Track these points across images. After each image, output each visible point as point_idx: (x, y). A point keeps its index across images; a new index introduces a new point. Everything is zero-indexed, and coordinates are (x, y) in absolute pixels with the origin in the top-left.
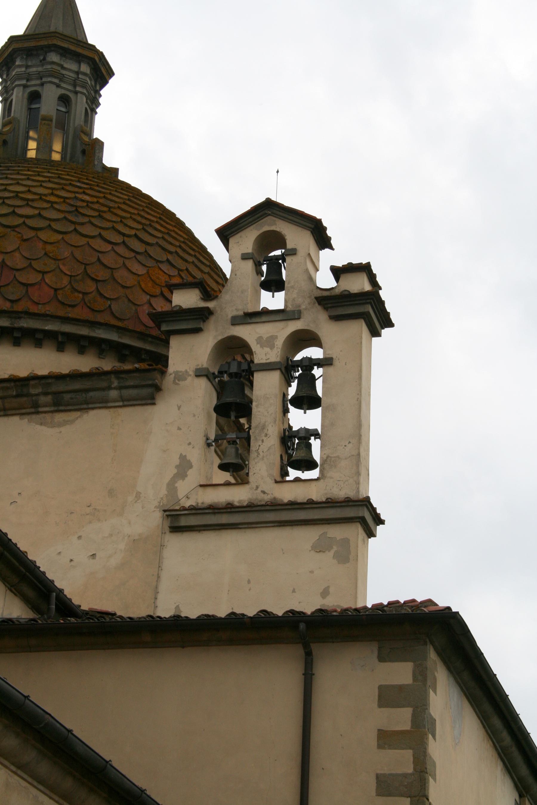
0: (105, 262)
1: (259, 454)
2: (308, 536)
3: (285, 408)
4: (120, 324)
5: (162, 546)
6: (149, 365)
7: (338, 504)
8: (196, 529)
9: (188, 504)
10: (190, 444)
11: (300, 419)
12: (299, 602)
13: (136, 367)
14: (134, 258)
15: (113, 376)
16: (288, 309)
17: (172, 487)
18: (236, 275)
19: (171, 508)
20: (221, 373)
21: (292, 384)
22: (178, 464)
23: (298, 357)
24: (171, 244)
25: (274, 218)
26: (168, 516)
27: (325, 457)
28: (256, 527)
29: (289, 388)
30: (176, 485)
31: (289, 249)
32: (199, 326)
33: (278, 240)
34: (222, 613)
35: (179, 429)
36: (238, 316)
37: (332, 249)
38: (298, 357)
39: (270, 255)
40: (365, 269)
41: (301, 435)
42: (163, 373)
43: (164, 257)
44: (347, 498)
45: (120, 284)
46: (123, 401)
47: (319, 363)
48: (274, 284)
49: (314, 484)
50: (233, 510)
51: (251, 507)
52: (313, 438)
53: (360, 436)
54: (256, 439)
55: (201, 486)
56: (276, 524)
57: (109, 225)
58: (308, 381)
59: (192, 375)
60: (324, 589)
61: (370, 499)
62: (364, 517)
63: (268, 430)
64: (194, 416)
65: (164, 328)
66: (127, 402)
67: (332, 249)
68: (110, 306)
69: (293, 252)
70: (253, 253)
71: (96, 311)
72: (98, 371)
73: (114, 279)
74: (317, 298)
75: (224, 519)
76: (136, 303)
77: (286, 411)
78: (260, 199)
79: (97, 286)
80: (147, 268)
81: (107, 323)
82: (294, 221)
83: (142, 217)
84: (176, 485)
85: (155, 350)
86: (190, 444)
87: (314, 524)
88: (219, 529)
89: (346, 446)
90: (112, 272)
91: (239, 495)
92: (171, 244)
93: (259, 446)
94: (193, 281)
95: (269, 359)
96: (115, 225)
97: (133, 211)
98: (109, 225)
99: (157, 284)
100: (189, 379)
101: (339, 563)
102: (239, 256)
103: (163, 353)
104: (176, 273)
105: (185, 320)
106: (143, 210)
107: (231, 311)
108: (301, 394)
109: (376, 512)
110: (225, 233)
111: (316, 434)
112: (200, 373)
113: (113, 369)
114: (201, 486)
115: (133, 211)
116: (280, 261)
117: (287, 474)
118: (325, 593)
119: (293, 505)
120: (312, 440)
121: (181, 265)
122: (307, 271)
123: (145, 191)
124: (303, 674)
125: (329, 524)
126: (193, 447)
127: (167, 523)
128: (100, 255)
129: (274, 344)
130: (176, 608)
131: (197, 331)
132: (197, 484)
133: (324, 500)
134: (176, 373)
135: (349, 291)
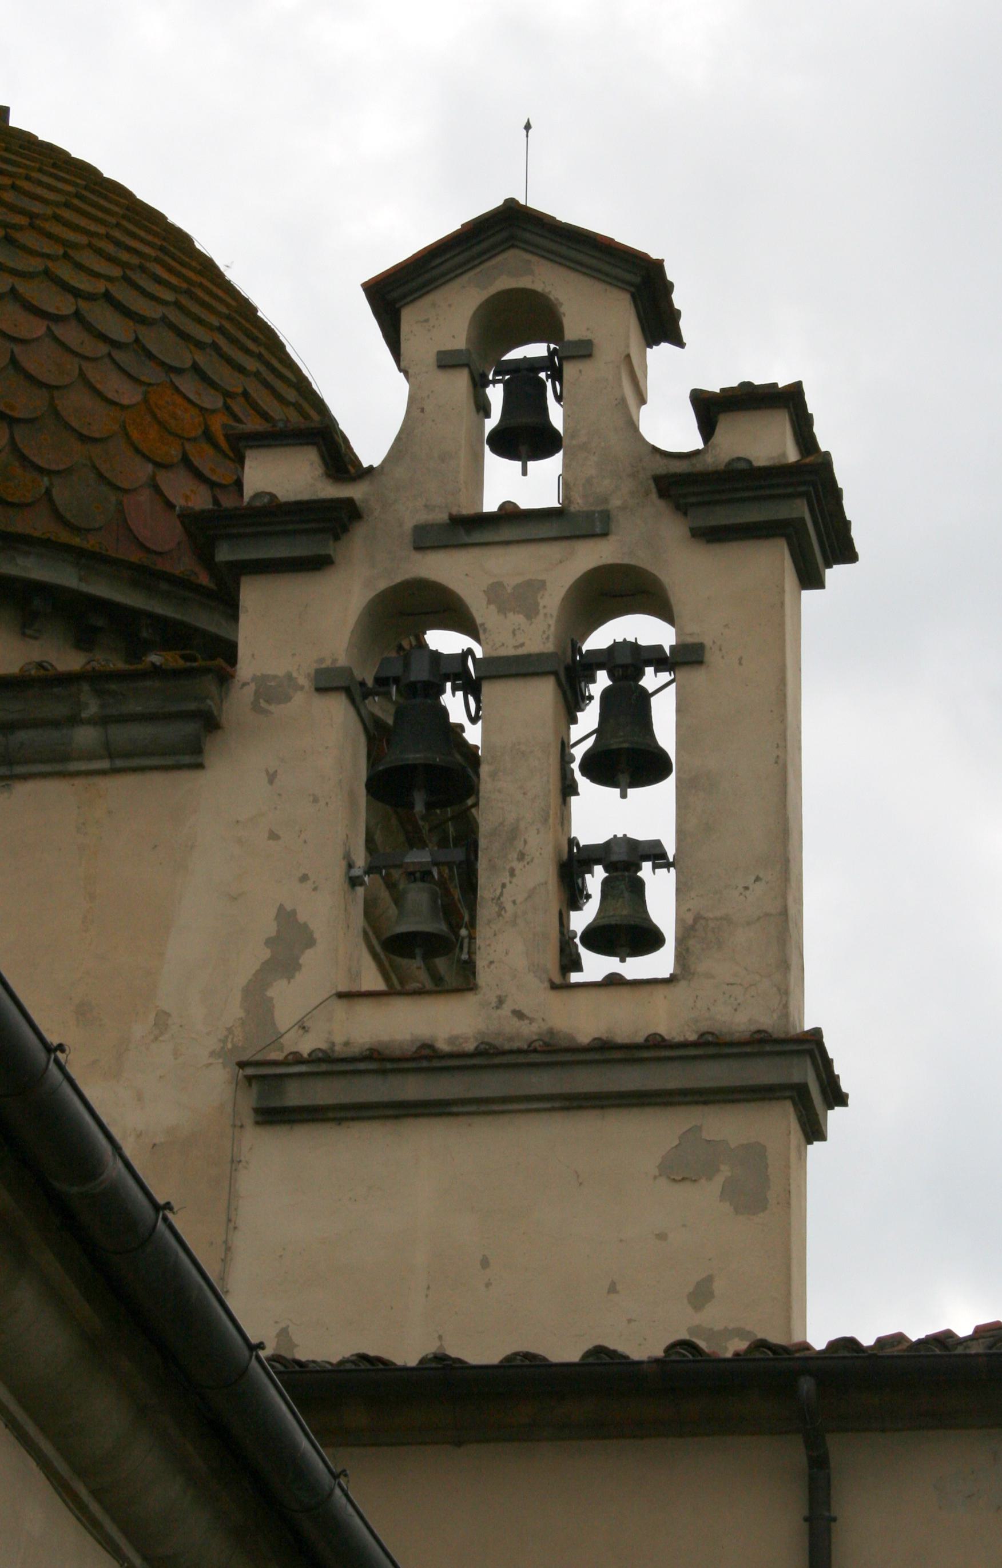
0: (32, 368)
1: (502, 908)
2: (645, 1138)
3: (568, 782)
4: (77, 541)
5: (235, 1162)
6: (186, 658)
7: (735, 1050)
8: (331, 1115)
9: (306, 1046)
10: (304, 878)
11: (599, 813)
12: (630, 1321)
13: (153, 664)
14: (107, 360)
15: (86, 687)
16: (573, 508)
17: (256, 998)
18: (422, 410)
19: (259, 1057)
20: (382, 681)
21: (579, 714)
22: (273, 934)
23: (599, 639)
24: (200, 321)
25: (528, 257)
26: (249, 1079)
27: (689, 919)
28: (503, 1112)
29: (572, 726)
30: (270, 993)
31: (570, 342)
32: (322, 552)
33: (535, 316)
34: (407, 1353)
35: (273, 836)
36: (432, 525)
37: (679, 343)
38: (599, 639)
39: (504, 358)
40: (790, 400)
41: (614, 858)
42: (225, 678)
43: (184, 357)
44: (759, 1032)
45: (73, 430)
46: (111, 756)
47: (657, 658)
48: (525, 438)
49: (661, 991)
50: (436, 1063)
51: (487, 1057)
52: (647, 866)
53: (787, 861)
54: (493, 868)
55: (341, 995)
56: (557, 1104)
57: (35, 264)
58: (628, 707)
59: (307, 688)
60: (698, 1285)
61: (821, 1037)
62: (800, 1081)
63: (525, 842)
64: (316, 800)
65: (224, 554)
66: (123, 760)
67: (679, 343)
68: (48, 492)
69: (583, 351)
70: (468, 350)
71: (11, 505)
72: (42, 672)
73: (57, 415)
74: (658, 479)
75: (412, 1088)
76: (119, 484)
77: (569, 789)
78: (490, 202)
79: (12, 438)
80: (144, 388)
81: (49, 539)
82: (581, 264)
83: (118, 243)
84: (270, 993)
85: (178, 617)
86: (304, 878)
87: (665, 1104)
88: (396, 1117)
89: (746, 888)
90: (52, 398)
91: (445, 1021)
92: (200, 321)
93: (504, 886)
94: (303, 426)
95: (522, 645)
96: (50, 264)
97: (93, 227)
98: (35, 264)
99: (170, 433)
100: (299, 698)
101: (737, 1211)
102: (431, 359)
103: (198, 624)
104: (220, 404)
105: (285, 533)
106: (118, 225)
107: (412, 512)
108: (615, 744)
109: (832, 1071)
110: (392, 296)
111: (655, 853)
112: (328, 682)
113: (89, 667)
114: (341, 995)
115: (93, 227)
116: (542, 375)
117: (576, 965)
118: (701, 1295)
119: (605, 1051)
120: (646, 871)
121: (233, 382)
122: (623, 402)
123: (109, 172)
124: (806, 1519)
125: (705, 1103)
126: (315, 889)
127: (248, 1101)
128: (17, 349)
129: (537, 604)
130: (278, 1335)
131: (319, 563)
132: (334, 992)
133: (692, 1037)
134: (262, 680)
135: (749, 462)
